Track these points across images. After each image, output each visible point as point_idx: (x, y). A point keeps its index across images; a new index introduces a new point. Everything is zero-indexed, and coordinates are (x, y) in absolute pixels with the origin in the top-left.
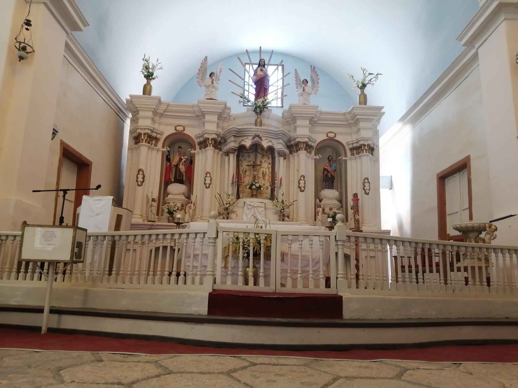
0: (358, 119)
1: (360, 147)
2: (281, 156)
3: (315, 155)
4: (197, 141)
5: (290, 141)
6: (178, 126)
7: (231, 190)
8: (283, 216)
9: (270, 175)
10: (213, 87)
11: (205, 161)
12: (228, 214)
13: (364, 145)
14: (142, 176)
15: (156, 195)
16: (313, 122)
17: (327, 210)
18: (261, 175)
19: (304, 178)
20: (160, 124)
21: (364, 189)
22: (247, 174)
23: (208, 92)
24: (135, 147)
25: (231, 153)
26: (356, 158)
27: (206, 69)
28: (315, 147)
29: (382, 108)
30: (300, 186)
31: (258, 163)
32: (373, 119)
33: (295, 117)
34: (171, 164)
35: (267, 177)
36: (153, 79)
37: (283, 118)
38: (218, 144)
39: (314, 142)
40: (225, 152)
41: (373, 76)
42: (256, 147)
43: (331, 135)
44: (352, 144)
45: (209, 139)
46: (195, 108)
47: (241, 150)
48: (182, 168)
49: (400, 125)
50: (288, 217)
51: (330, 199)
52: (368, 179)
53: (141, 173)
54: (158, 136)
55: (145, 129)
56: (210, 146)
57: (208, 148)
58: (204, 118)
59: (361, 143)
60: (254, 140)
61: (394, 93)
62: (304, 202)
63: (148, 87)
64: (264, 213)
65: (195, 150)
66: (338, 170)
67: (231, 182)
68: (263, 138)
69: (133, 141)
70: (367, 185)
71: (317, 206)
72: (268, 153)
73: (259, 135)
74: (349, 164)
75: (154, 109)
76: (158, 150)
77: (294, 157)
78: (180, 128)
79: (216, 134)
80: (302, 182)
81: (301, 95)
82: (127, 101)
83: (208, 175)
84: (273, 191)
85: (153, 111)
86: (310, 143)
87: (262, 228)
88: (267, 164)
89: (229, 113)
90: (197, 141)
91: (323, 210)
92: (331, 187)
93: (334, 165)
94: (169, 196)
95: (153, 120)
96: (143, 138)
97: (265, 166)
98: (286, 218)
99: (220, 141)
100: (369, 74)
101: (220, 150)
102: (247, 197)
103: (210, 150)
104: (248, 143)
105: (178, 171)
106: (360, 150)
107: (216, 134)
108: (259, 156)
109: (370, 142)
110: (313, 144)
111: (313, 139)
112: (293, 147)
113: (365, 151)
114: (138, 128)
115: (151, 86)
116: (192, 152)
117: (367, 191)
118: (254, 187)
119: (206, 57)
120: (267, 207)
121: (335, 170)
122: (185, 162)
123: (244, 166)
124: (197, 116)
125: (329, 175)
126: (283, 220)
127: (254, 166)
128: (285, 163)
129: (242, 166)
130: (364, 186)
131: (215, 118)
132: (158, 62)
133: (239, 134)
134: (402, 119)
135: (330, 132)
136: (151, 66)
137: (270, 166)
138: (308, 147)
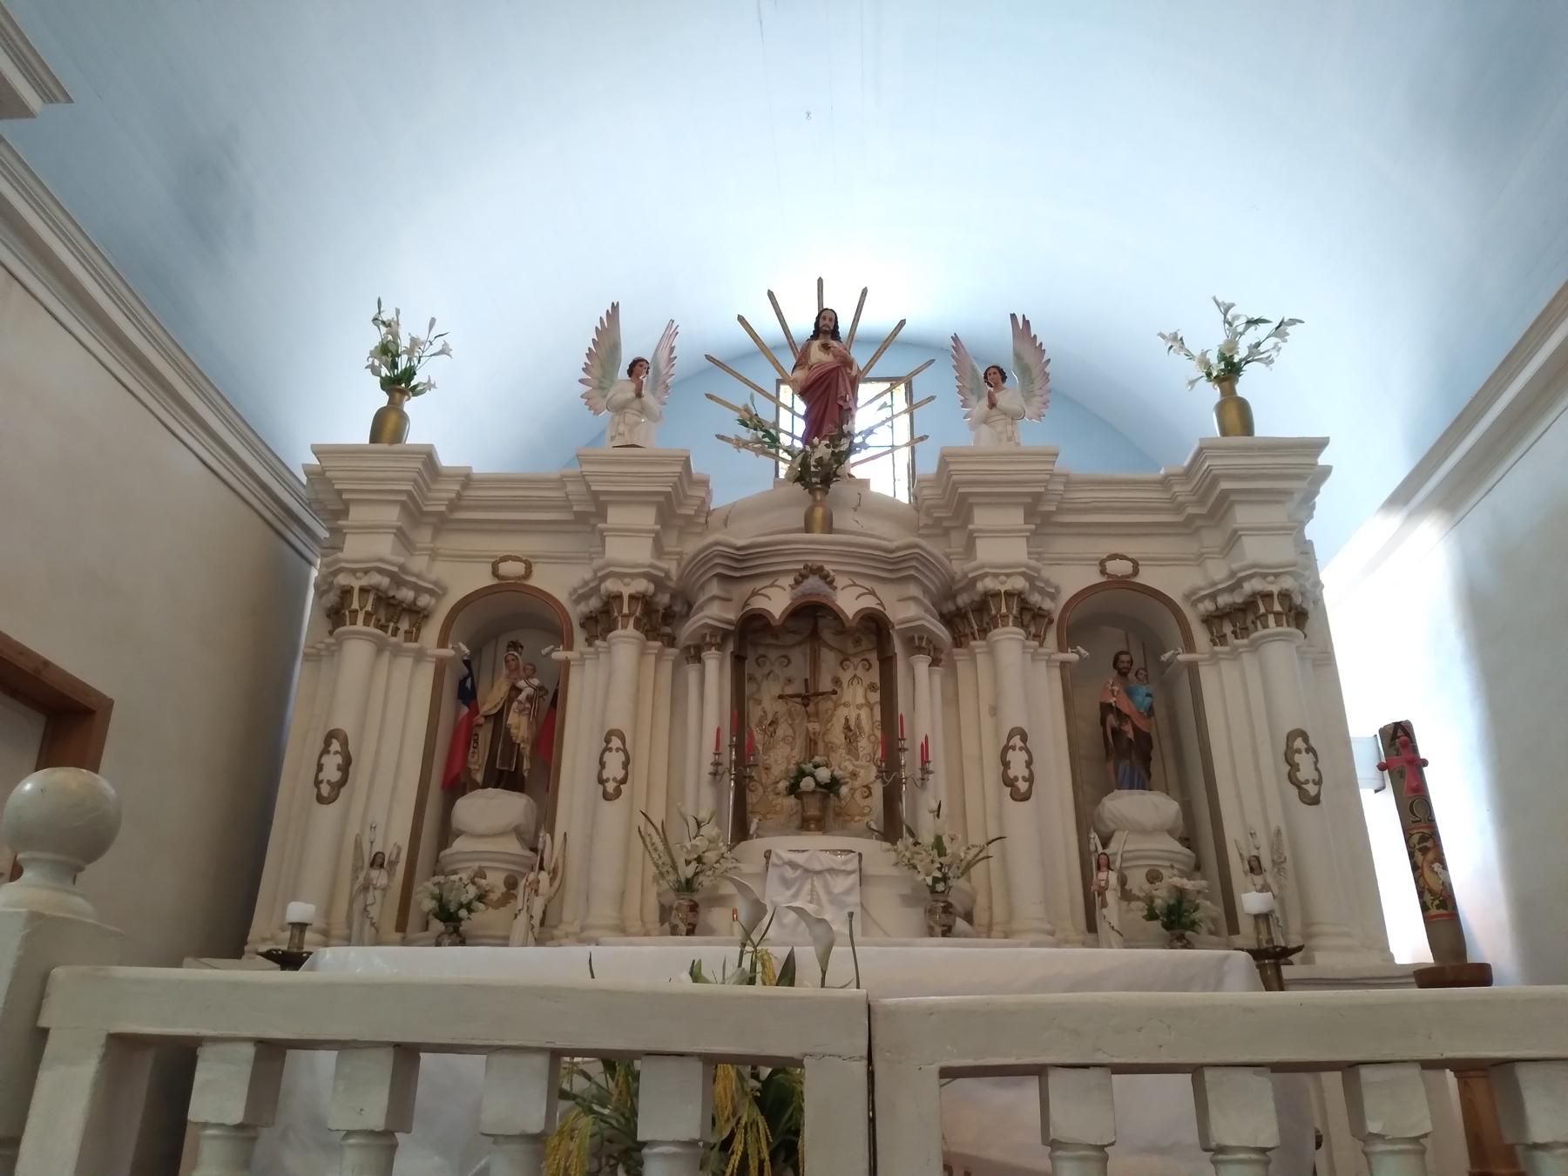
0: (1226, 494)
1: (1249, 605)
2: (920, 650)
3: (1062, 649)
4: (576, 612)
5: (951, 595)
6: (504, 559)
7: (704, 799)
8: (944, 912)
9: (878, 733)
10: (643, 411)
11: (608, 687)
12: (694, 908)
13: (1267, 596)
14: (339, 759)
15: (396, 836)
16: (1045, 511)
17: (1137, 881)
18: (837, 736)
19: (1024, 738)
20: (434, 555)
21: (1292, 778)
22: (780, 732)
23: (622, 428)
24: (328, 646)
25: (710, 645)
26: (1235, 655)
27: (615, 348)
28: (1056, 617)
29: (1319, 445)
30: (1011, 773)
31: (826, 685)
32: (1288, 493)
33: (964, 496)
34: (474, 711)
35: (864, 744)
36: (415, 391)
37: (917, 509)
38: (659, 617)
39: (1053, 597)
40: (688, 648)
41: (1262, 331)
42: (811, 615)
43: (1119, 568)
44: (1213, 597)
45: (619, 597)
46: (570, 488)
47: (751, 631)
48: (519, 725)
49: (1395, 520)
50: (968, 917)
51: (1143, 831)
52: (1303, 735)
53: (335, 746)
54: (424, 600)
55: (366, 572)
56: (624, 627)
57: (619, 632)
58: (604, 518)
59: (1248, 587)
60: (800, 589)
61: (1353, 395)
62: (1033, 841)
63: (393, 418)
64: (854, 898)
65: (570, 647)
66: (1160, 712)
67: (710, 769)
68: (841, 581)
69: (326, 625)
70: (1304, 760)
71: (1091, 864)
72: (865, 644)
73: (821, 569)
74: (1207, 676)
75: (408, 493)
76: (420, 656)
77: (973, 657)
78: (511, 569)
79: (647, 576)
80: (1017, 759)
81: (986, 421)
82: (315, 475)
83: (616, 742)
84: (891, 798)
85: (403, 504)
86: (1035, 598)
87: (788, 975)
88: (860, 691)
89: (704, 502)
90: (576, 612)
91: (1123, 881)
92: (1141, 780)
93: (1143, 690)
94: (459, 845)
95: (401, 535)
96: (355, 605)
97: (855, 701)
98: (960, 924)
99: (668, 608)
100: (1250, 322)
101: (671, 641)
102: (783, 830)
103: (625, 643)
104: (777, 601)
105: (497, 739)
106: (1250, 617)
107: (647, 576)
108: (828, 658)
109: (1288, 583)
110: (1047, 605)
111: (1047, 582)
112: (967, 616)
113: (1271, 618)
114: (341, 570)
115: (403, 419)
116: (555, 655)
117: (1312, 789)
118: (807, 784)
119: (615, 307)
120: (870, 869)
121: (1150, 711)
122: (529, 699)
123: (768, 699)
124: (581, 518)
125: (1128, 728)
126: (947, 931)
127: (809, 697)
128: (937, 679)
129: (759, 702)
130: (1294, 767)
131: (646, 517)
132: (435, 332)
133: (740, 566)
134: (1400, 498)
135: (1114, 557)
136: (404, 343)
137: (875, 697)
138: (1030, 616)
